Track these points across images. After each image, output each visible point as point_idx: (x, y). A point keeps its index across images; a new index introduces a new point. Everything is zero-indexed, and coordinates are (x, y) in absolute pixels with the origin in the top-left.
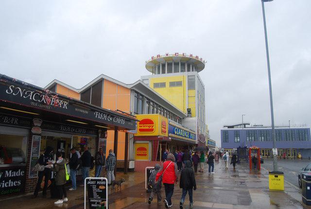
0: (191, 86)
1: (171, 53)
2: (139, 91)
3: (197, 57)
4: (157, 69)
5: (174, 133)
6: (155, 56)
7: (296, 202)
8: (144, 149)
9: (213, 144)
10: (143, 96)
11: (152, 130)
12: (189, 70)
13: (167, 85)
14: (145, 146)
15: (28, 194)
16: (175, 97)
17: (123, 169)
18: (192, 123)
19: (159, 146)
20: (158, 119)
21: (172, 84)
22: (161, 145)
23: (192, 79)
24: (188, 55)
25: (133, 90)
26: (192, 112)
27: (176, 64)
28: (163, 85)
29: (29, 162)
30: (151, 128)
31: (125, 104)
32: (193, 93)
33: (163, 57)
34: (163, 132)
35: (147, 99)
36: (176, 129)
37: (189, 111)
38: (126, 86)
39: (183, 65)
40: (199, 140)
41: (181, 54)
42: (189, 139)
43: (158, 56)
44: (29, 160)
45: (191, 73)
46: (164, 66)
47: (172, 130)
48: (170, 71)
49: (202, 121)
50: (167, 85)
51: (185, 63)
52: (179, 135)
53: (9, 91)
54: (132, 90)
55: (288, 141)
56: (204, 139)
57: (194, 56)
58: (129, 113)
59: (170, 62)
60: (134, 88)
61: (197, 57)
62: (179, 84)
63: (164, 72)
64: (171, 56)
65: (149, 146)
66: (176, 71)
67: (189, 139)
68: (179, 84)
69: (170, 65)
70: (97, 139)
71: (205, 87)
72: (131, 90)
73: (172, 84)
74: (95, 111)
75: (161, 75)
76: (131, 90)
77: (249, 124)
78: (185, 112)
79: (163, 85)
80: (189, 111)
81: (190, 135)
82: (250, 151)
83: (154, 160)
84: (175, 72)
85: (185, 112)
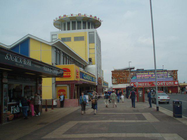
0: (91, 41)
1: (75, 14)
2: (58, 48)
3: (95, 17)
4: (63, 26)
5: (83, 78)
6: (62, 16)
7: (169, 117)
8: (63, 91)
9: (107, 84)
10: (59, 50)
11: (69, 76)
12: (89, 28)
13: (72, 39)
14: (64, 88)
15: (4, 124)
16: (79, 49)
17: (45, 106)
18: (92, 68)
19: (75, 87)
20: (73, 68)
21: (76, 39)
22: (76, 87)
23: (91, 33)
24: (88, 16)
25: (54, 46)
26: (92, 60)
27: (79, 22)
28: (69, 39)
29: (3, 102)
30: (68, 75)
31: (47, 57)
32: (94, 45)
33: (68, 16)
34: (77, 77)
35: (63, 53)
36: (84, 75)
37: (90, 60)
38: (48, 43)
39: (84, 23)
40: (98, 82)
41: (83, 14)
42: (92, 82)
43: (65, 16)
44: (2, 101)
45: (91, 30)
46: (69, 23)
47: (82, 75)
48: (74, 28)
49: (99, 67)
50: (72, 39)
51: (86, 22)
52: (86, 79)
53: (7, 58)
54: (53, 47)
55: (71, 74)
56: (101, 82)
57: (93, 16)
58: (51, 64)
59: (74, 20)
60: (54, 45)
61: (95, 17)
62: (82, 38)
63: (69, 29)
64: (75, 16)
65: (67, 89)
66: (79, 28)
67: (92, 82)
68: (82, 38)
69: (74, 23)
70: (37, 84)
71: (101, 41)
72: (52, 46)
73: (76, 39)
74: (43, 66)
75: (67, 32)
76: (52, 46)
77: (134, 69)
78: (87, 61)
79: (69, 39)
80: (90, 60)
81: (92, 78)
82: (138, 88)
83: (70, 99)
84: (78, 29)
85: (87, 61)
